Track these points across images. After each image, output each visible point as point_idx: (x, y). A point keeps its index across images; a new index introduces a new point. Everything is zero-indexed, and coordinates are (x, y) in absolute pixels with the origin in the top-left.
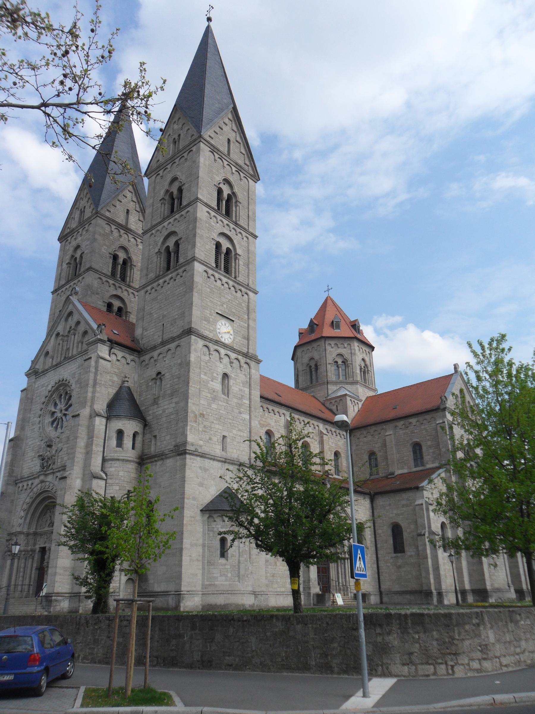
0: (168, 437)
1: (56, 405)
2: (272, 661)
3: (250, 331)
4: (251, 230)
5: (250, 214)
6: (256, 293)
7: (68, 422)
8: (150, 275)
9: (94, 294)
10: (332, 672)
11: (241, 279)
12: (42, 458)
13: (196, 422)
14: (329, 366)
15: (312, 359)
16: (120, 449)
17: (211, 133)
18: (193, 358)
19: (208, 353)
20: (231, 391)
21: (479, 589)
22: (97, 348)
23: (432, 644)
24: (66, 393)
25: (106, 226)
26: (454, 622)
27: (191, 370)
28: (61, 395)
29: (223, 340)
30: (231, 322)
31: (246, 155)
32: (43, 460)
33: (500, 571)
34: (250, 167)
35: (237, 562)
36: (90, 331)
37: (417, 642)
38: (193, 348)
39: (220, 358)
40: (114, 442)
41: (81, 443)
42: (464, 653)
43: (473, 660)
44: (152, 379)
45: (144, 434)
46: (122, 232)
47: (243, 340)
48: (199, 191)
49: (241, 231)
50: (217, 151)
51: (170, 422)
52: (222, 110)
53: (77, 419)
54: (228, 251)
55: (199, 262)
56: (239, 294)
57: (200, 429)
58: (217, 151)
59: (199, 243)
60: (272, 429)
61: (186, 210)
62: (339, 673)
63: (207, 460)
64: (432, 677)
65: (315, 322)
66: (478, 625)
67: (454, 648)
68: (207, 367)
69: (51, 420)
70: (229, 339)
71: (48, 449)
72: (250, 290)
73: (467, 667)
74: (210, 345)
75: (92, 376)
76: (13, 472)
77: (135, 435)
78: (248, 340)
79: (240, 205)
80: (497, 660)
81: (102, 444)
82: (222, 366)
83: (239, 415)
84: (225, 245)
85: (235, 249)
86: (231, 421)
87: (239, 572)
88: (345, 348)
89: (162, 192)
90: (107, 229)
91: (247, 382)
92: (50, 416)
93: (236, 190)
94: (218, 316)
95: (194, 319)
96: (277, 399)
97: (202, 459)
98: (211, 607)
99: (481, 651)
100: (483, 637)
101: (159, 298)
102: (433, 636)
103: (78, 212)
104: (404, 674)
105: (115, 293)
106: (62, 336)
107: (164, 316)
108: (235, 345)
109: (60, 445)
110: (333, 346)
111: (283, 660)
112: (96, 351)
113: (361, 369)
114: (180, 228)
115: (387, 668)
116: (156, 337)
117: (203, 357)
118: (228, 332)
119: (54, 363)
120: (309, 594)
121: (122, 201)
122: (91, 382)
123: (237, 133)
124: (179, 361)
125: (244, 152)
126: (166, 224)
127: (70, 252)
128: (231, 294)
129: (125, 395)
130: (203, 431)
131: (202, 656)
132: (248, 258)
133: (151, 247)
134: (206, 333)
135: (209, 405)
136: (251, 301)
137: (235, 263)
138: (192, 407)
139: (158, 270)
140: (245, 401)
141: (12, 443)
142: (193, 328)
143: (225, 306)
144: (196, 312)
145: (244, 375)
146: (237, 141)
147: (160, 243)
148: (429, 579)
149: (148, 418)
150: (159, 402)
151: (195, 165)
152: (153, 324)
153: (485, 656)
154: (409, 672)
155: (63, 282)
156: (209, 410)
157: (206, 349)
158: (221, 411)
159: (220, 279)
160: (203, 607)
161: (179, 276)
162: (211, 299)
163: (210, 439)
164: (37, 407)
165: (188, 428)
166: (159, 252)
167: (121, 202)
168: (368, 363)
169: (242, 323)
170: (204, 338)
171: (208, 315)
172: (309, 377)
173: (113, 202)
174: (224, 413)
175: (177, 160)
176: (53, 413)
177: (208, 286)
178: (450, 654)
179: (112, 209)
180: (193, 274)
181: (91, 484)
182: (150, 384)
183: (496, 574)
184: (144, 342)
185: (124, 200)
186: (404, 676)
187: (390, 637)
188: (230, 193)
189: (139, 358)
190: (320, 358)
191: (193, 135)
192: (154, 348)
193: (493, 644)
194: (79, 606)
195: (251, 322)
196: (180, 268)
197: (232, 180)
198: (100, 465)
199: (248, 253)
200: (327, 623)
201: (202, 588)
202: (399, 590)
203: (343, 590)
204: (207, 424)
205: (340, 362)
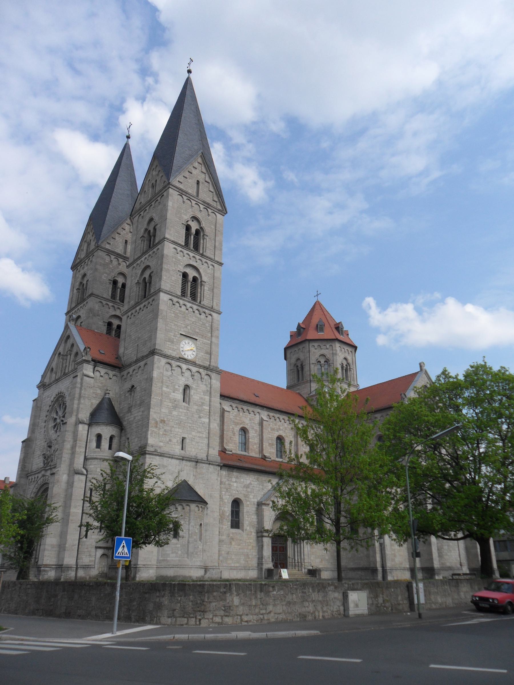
0: (136, 440)
1: (57, 412)
2: (101, 614)
3: (213, 347)
4: (217, 259)
5: (217, 244)
6: (219, 313)
7: (63, 428)
8: (131, 303)
9: (95, 316)
10: (131, 621)
11: (205, 302)
12: (45, 456)
13: (157, 427)
14: (312, 366)
15: (298, 359)
16: (99, 449)
17: (180, 178)
18: (155, 374)
19: (170, 369)
20: (191, 400)
21: (428, 568)
22: (83, 366)
23: (188, 604)
24: (64, 404)
25: (107, 257)
26: (206, 590)
27: (154, 385)
28: (60, 405)
29: (186, 357)
30: (195, 341)
31: (214, 193)
32: (45, 458)
33: (453, 551)
34: (218, 203)
35: (187, 542)
36: (79, 353)
37: (179, 602)
38: (155, 366)
39: (182, 372)
40: (94, 444)
41: (68, 446)
42: (210, 611)
43: (216, 616)
44: (128, 391)
45: (121, 437)
46: (121, 260)
47: (205, 355)
48: (167, 231)
49: (207, 261)
50: (185, 194)
51: (138, 427)
52: (191, 156)
53: (65, 426)
54: (195, 279)
55: (165, 293)
56: (203, 316)
57: (161, 433)
58: (185, 194)
59: (165, 276)
60: (246, 426)
61: (157, 248)
62: (134, 622)
63: (165, 459)
64: (185, 626)
65: (302, 326)
66: (225, 593)
67: (203, 607)
68: (170, 381)
69: (53, 424)
70: (192, 356)
71: (49, 449)
72: (213, 311)
73: (211, 621)
74: (173, 362)
75: (77, 390)
76: (25, 468)
77: (111, 438)
78: (210, 354)
79: (207, 238)
80: (239, 617)
81: (84, 446)
82: (183, 379)
83: (199, 419)
84: (191, 273)
85: (201, 277)
86: (190, 425)
87: (188, 550)
88: (327, 349)
89: (143, 230)
90: (107, 259)
91: (207, 391)
92: (53, 421)
93: (204, 225)
94: (182, 336)
95: (158, 341)
96: (253, 399)
97: (161, 458)
98: (162, 577)
99: (224, 611)
100: (228, 601)
101: (136, 322)
102: (189, 599)
103: (86, 245)
104: (168, 623)
105: (114, 313)
106: (63, 355)
107: (139, 338)
108: (197, 360)
109: (57, 446)
110: (316, 347)
111: (107, 613)
112: (82, 370)
113: (342, 367)
114: (152, 263)
115: (159, 619)
116: (133, 355)
117: (165, 373)
118: (191, 350)
119: (57, 378)
120: (262, 569)
121: (121, 233)
122: (77, 396)
123: (207, 174)
124: (146, 377)
125: (213, 190)
126: (143, 259)
127: (79, 280)
128: (196, 316)
129: (106, 405)
130: (163, 434)
131: (66, 609)
132: (213, 283)
133: (133, 278)
134: (170, 352)
135: (170, 412)
136: (214, 321)
137: (201, 289)
138: (153, 415)
139: (137, 298)
140: (204, 407)
141: (24, 443)
142: (157, 349)
143: (189, 327)
144: (160, 336)
145: (206, 385)
146: (206, 181)
147: (139, 275)
148: (375, 557)
149: (125, 423)
150: (132, 410)
151: (165, 206)
152: (131, 345)
153: (226, 614)
154: (171, 622)
155: (73, 305)
156: (169, 417)
157: (168, 366)
158: (181, 417)
159: (184, 305)
160: (157, 578)
161: (150, 304)
162: (176, 323)
163: (170, 440)
164: (44, 414)
165: (149, 432)
166: (138, 283)
167: (120, 234)
168: (350, 361)
169: (205, 340)
170: (166, 356)
171: (172, 337)
172: (296, 376)
173: (113, 236)
174: (185, 418)
175: (153, 203)
176: (56, 419)
177: (172, 312)
178: (200, 611)
179: (112, 242)
180: (159, 303)
181: (73, 478)
182: (127, 395)
183: (449, 554)
184: (125, 360)
185: (123, 233)
186: (168, 625)
187: (163, 599)
188: (198, 228)
189: (120, 373)
190: (305, 359)
191: (165, 182)
192: (130, 365)
193: (237, 606)
194: (62, 575)
195: (214, 339)
196: (150, 298)
197: (200, 217)
198: (82, 463)
199: (214, 279)
200: (133, 589)
201: (157, 563)
202: (353, 566)
203: (298, 567)
204: (168, 428)
205: (322, 362)
